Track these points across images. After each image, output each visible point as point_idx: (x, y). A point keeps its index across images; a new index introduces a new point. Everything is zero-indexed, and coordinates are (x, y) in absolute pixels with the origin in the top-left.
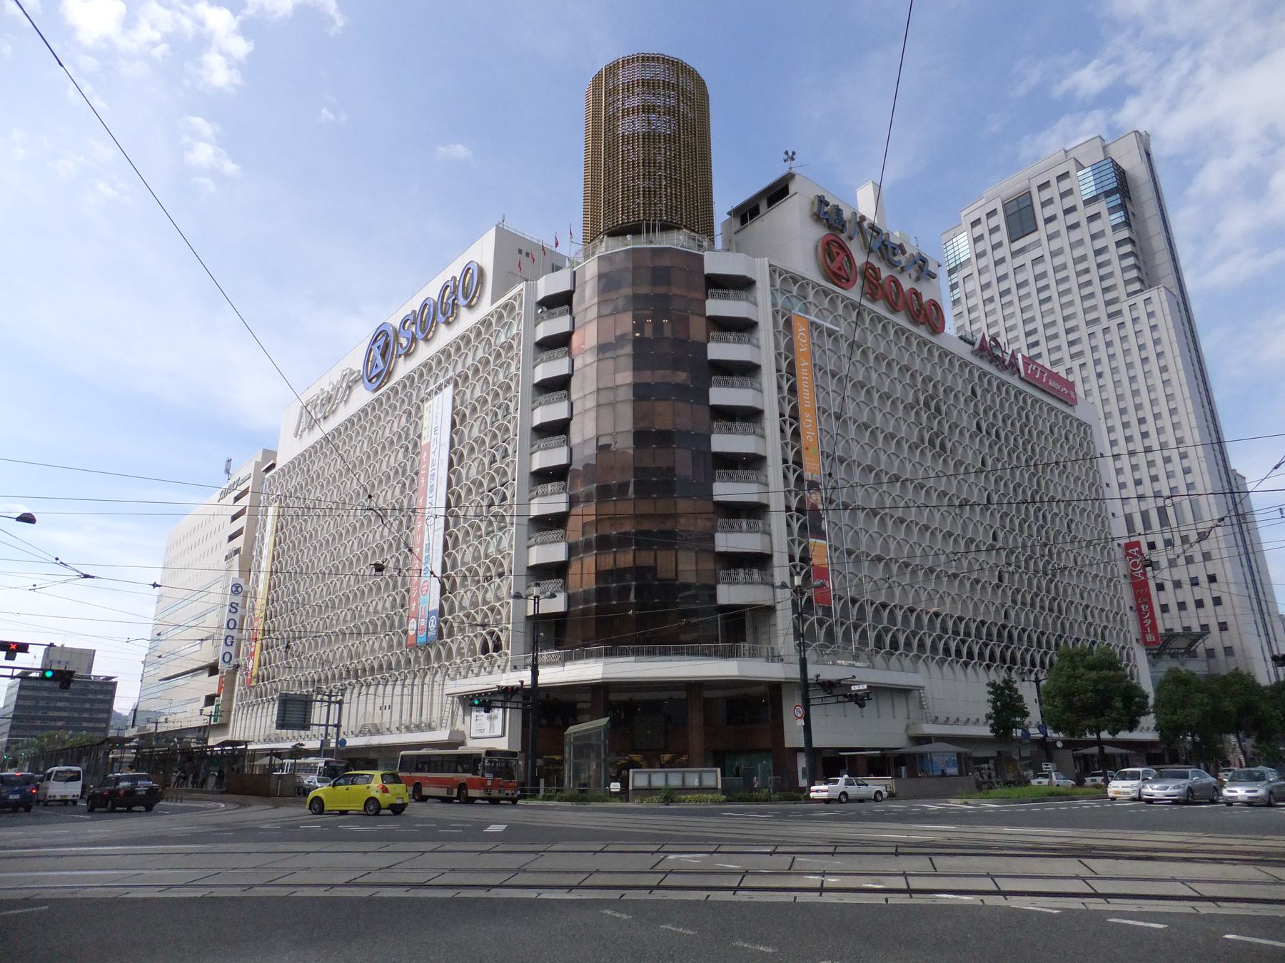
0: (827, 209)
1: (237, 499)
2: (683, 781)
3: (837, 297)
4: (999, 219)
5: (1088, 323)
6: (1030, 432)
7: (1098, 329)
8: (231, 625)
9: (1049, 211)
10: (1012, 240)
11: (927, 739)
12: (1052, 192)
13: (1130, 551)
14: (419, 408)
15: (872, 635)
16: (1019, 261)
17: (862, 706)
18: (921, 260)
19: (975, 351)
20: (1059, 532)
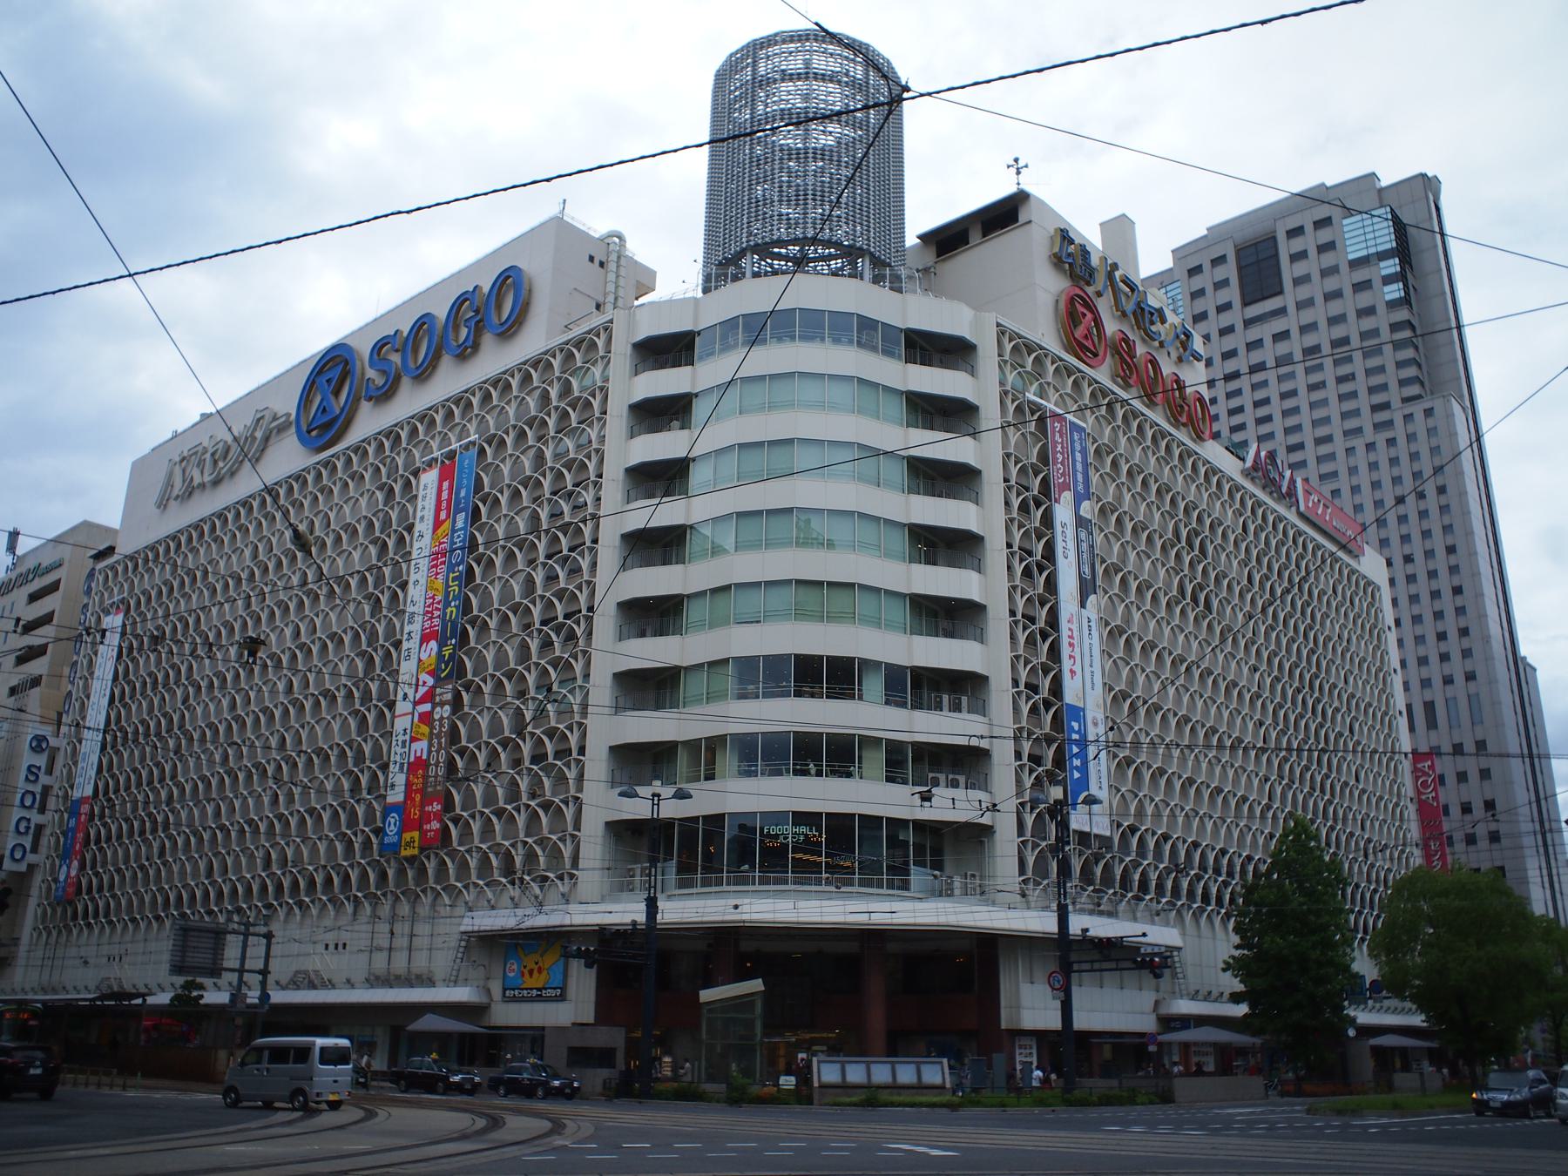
0: (1072, 248)
1: (34, 598)
2: (869, 1075)
3: (1083, 378)
4: (1230, 271)
5: (1346, 433)
6: (1205, 571)
7: (1359, 443)
8: (28, 803)
9: (1300, 269)
10: (1246, 303)
11: (1186, 1021)
12: (1308, 242)
13: (1419, 766)
14: (408, 484)
15: (1076, 865)
16: (1254, 334)
17: (1157, 976)
18: (1185, 334)
19: (1247, 469)
20: (1340, 734)
